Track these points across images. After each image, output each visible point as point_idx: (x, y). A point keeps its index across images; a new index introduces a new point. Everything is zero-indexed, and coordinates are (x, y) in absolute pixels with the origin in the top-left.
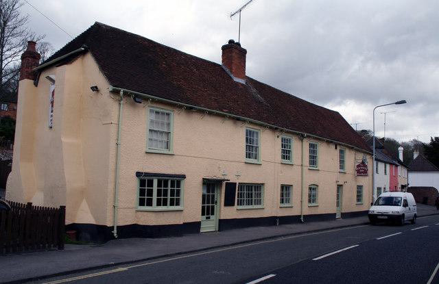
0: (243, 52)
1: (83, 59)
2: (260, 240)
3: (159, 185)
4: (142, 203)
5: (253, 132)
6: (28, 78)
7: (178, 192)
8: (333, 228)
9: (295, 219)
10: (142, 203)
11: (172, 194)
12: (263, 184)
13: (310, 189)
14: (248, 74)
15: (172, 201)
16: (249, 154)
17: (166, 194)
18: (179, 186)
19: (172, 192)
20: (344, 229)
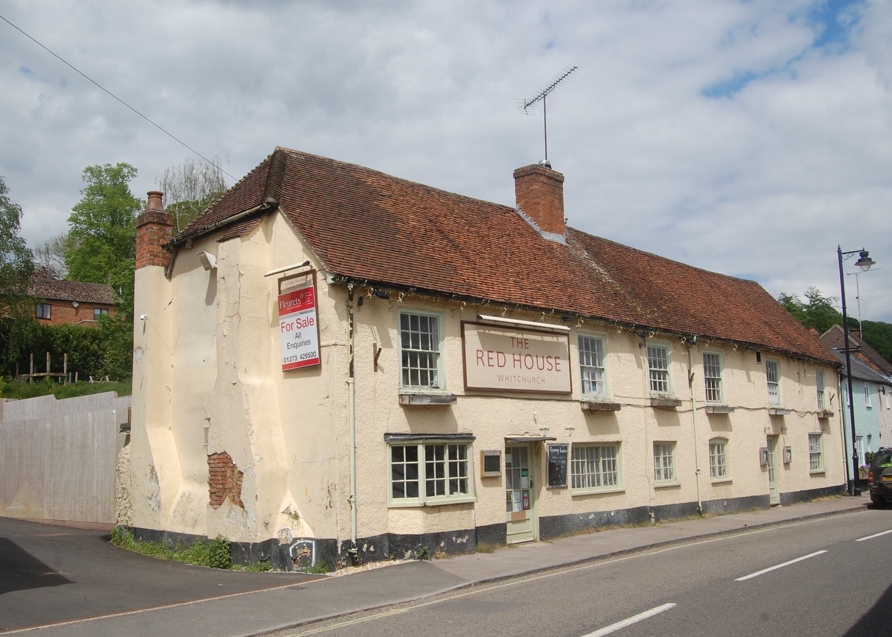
0: (557, 181)
1: (267, 223)
2: (720, 534)
3: (429, 456)
4: (398, 491)
5: (593, 341)
6: (153, 264)
7: (463, 466)
8: (765, 525)
9: (692, 510)
10: (398, 491)
11: (453, 472)
12: (675, 442)
13: (712, 447)
14: (569, 224)
15: (453, 484)
16: (414, 373)
17: (441, 473)
18: (463, 456)
19: (453, 467)
20: (782, 526)
